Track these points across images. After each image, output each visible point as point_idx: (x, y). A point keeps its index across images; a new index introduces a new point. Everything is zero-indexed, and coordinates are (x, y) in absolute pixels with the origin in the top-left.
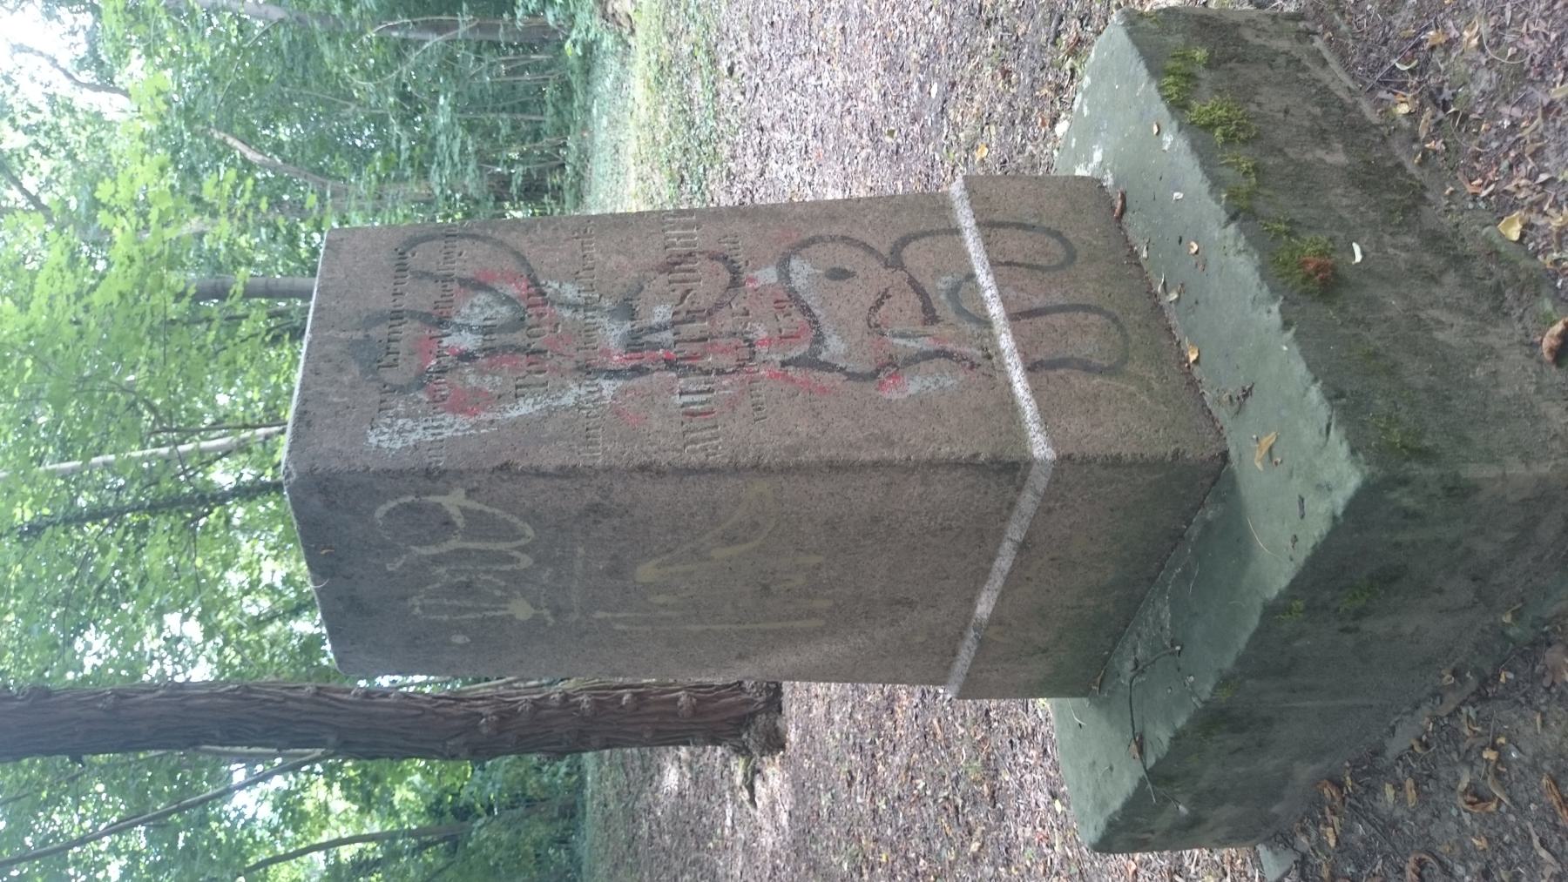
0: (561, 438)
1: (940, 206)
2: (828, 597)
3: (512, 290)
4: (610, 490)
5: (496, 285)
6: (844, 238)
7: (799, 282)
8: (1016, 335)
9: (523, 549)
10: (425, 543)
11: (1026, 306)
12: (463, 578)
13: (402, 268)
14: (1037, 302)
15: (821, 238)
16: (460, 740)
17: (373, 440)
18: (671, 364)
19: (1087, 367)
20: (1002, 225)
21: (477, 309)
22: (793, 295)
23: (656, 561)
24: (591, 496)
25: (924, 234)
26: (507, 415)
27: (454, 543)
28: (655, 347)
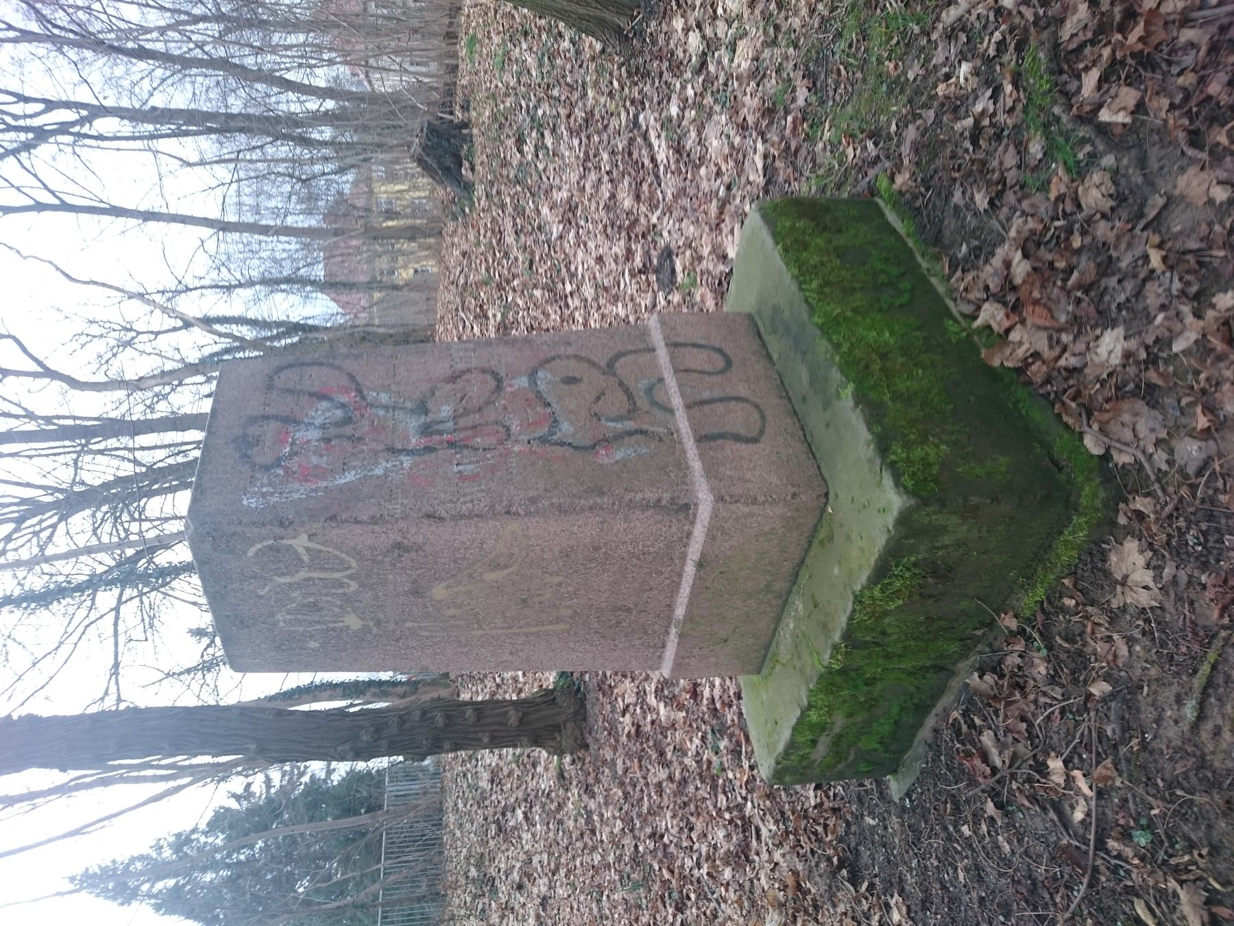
0: (372, 497)
1: (644, 333)
2: (569, 607)
3: (344, 399)
4: (408, 532)
5: (334, 396)
6: (575, 356)
7: (542, 386)
8: (691, 418)
9: (351, 577)
10: (283, 574)
11: (698, 398)
12: (311, 600)
13: (270, 387)
14: (706, 395)
15: (559, 357)
16: (347, 746)
17: (245, 502)
18: (451, 444)
19: (737, 438)
20: (685, 345)
21: (322, 413)
22: (539, 395)
23: (445, 584)
24: (394, 537)
25: (631, 352)
27: (303, 574)
28: (440, 433)
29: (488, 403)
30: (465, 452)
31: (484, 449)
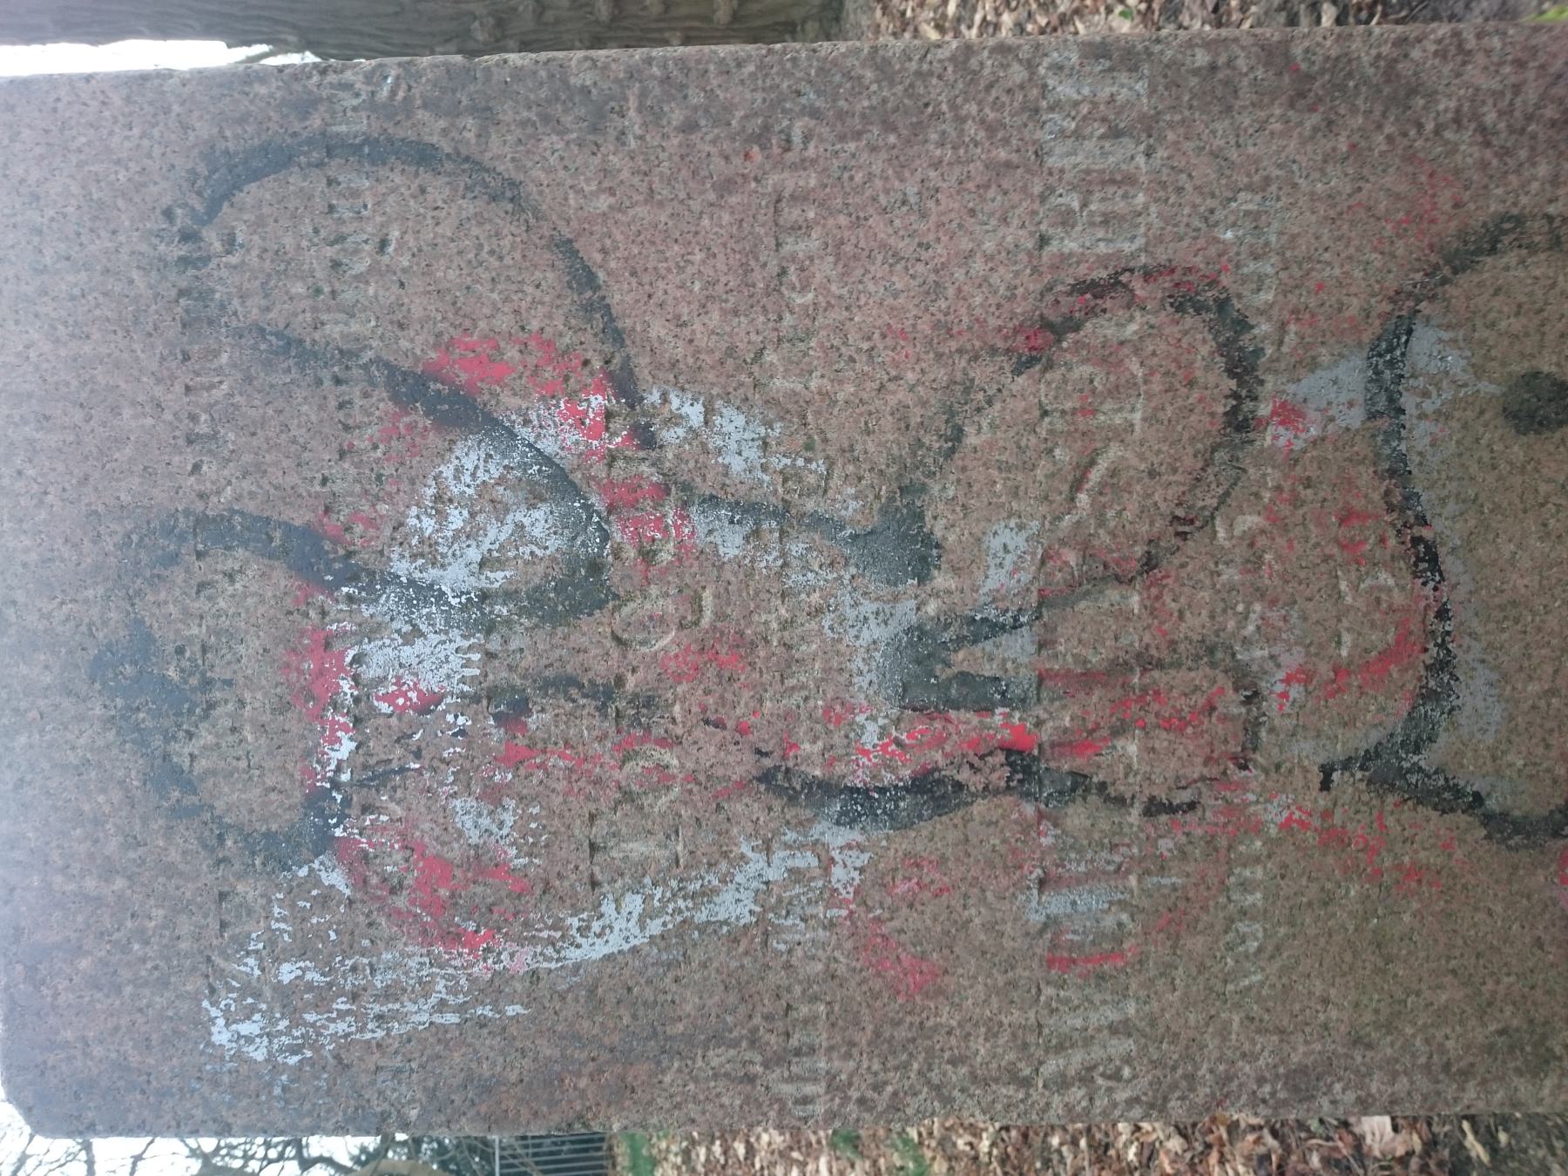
0: (717, 1039)
17: (221, 1035)
26: (573, 955)
29: (1186, 524)
30: (1077, 816)
31: (1154, 808)
